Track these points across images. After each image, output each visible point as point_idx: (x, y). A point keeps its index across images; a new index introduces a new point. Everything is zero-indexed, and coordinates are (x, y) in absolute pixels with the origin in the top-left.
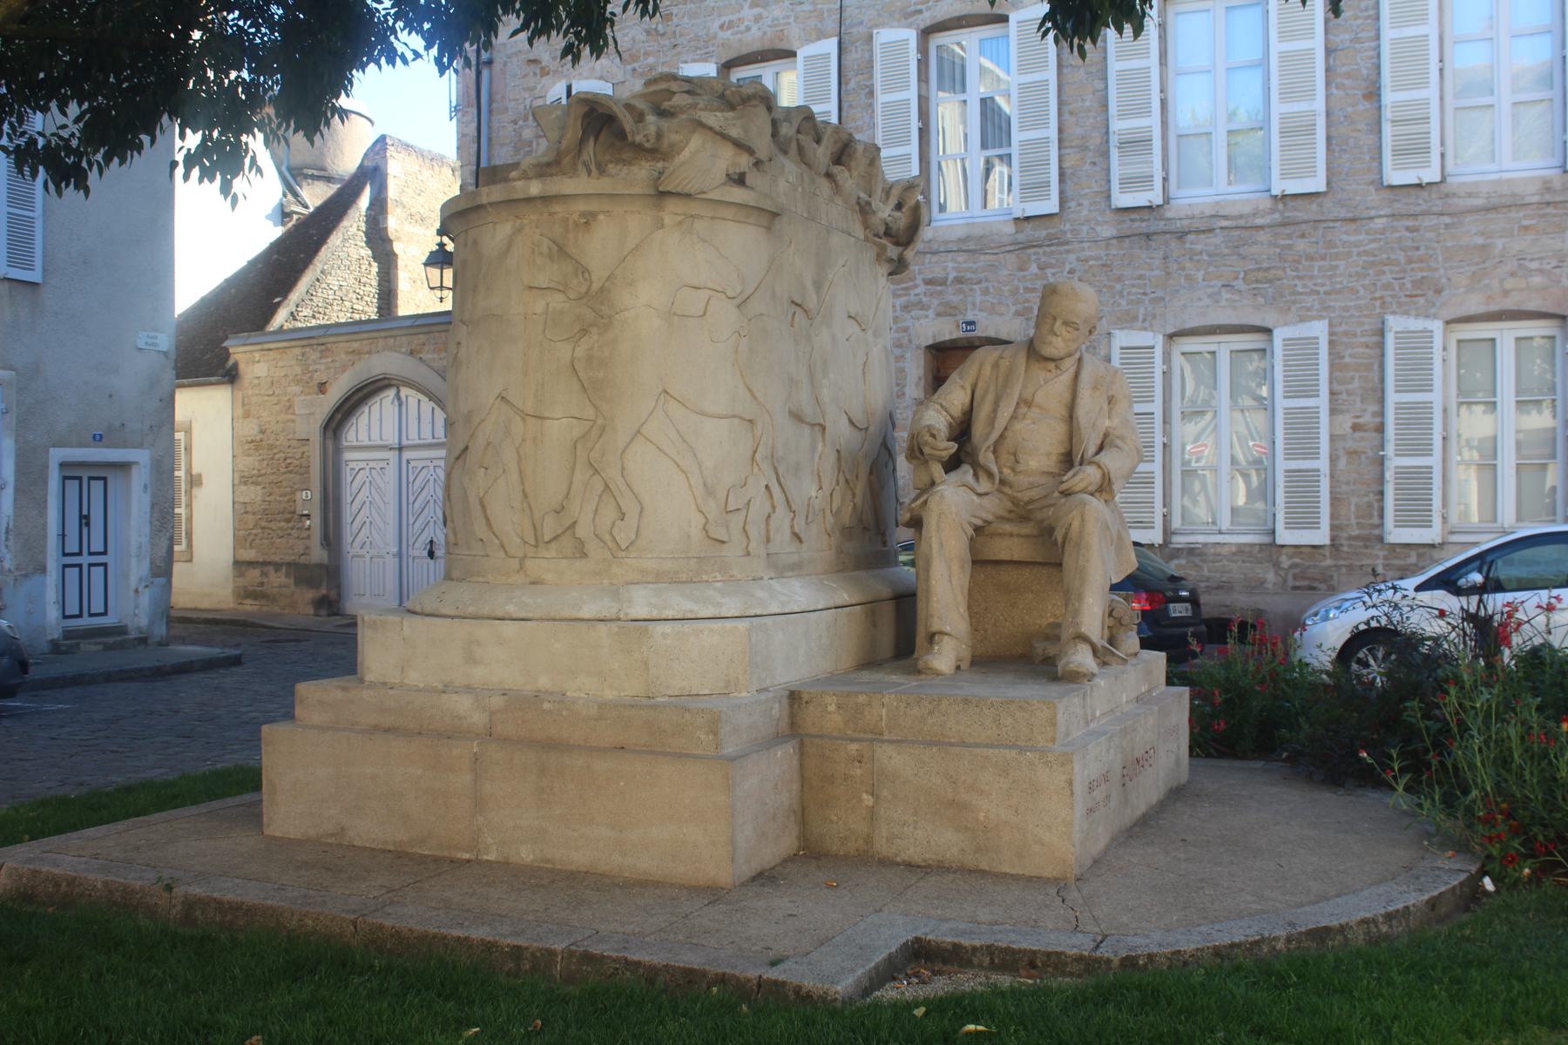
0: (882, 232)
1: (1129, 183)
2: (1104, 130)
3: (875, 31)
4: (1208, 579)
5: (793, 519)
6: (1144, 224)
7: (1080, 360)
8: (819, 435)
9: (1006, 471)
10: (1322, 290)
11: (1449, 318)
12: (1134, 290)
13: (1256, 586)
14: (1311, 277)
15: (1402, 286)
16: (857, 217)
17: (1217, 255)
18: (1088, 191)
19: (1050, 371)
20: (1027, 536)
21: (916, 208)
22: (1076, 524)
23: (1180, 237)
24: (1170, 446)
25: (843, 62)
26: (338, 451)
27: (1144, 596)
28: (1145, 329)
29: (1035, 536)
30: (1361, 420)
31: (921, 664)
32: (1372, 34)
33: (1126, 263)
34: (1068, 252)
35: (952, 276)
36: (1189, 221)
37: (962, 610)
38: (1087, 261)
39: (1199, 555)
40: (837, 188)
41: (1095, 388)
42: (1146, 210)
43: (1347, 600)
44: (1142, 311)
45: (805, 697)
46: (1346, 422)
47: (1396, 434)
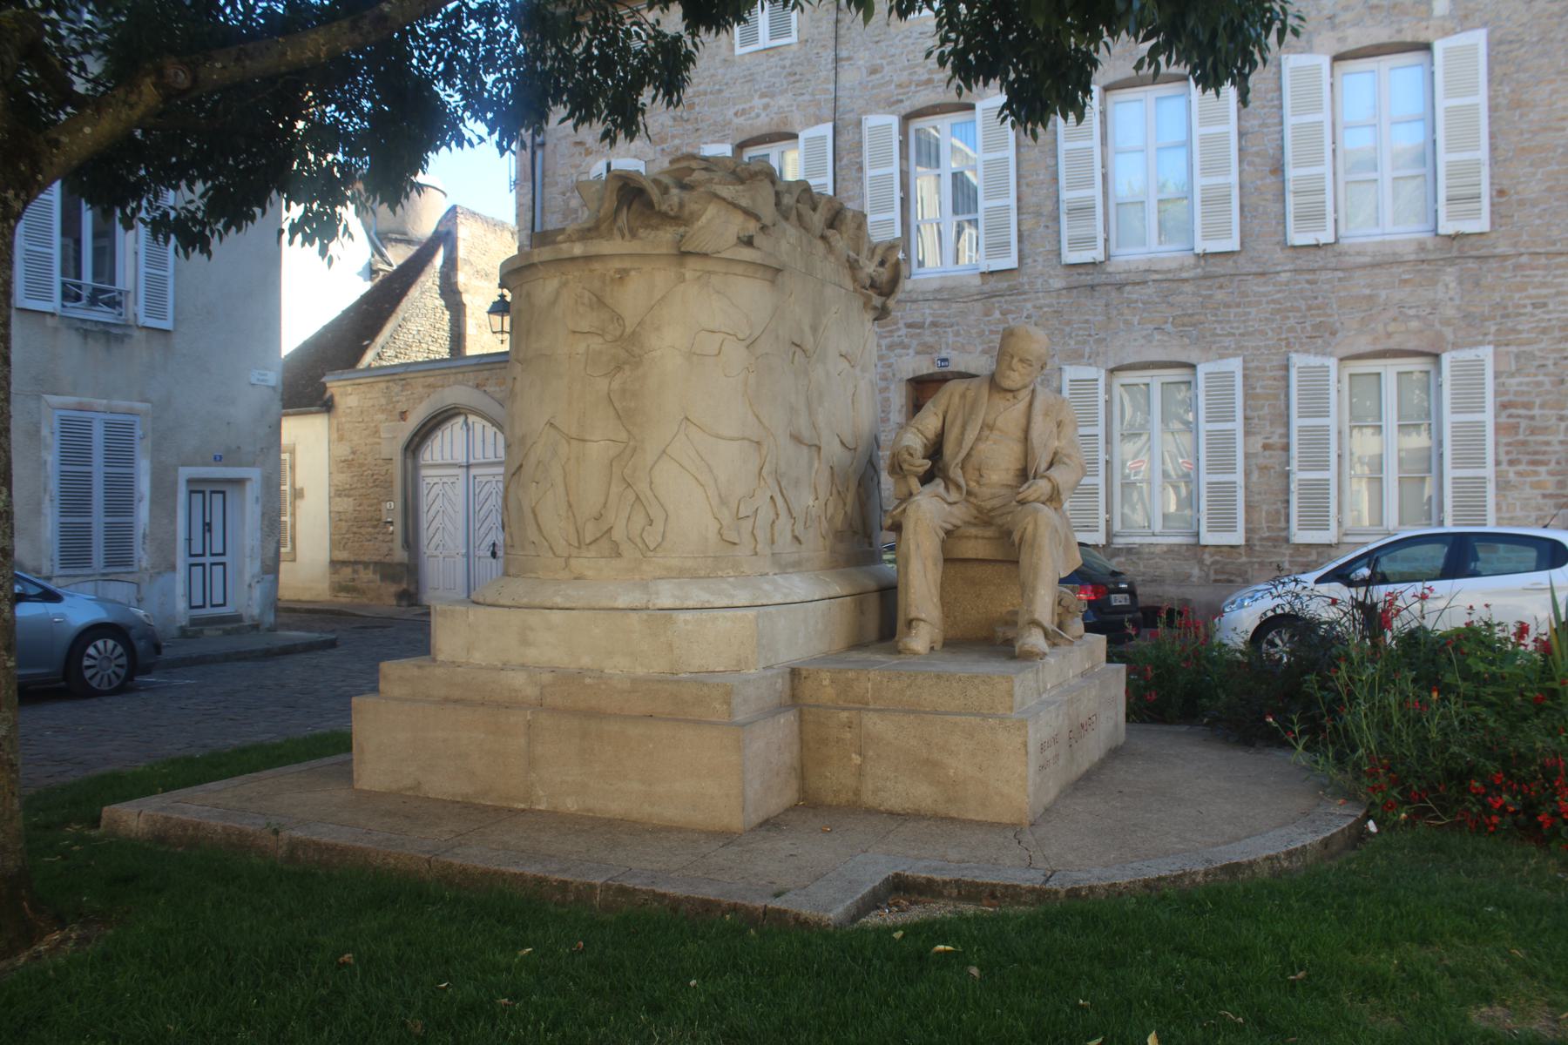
1: (1076, 243)
2: (1055, 199)
3: (864, 117)
4: (1144, 574)
5: (793, 525)
6: (1089, 278)
7: (1033, 391)
9: (973, 484)
10: (1237, 332)
11: (1342, 356)
12: (1081, 333)
13: (1184, 579)
16: (847, 272)
17: (1149, 303)
20: (989, 539)
22: (1030, 528)
24: (1112, 463)
26: (416, 468)
28: (1090, 365)
30: (1270, 441)
31: (901, 645)
32: (1276, 120)
34: (1025, 300)
40: (830, 248)
44: (1087, 350)
45: (804, 673)
46: (1257, 442)
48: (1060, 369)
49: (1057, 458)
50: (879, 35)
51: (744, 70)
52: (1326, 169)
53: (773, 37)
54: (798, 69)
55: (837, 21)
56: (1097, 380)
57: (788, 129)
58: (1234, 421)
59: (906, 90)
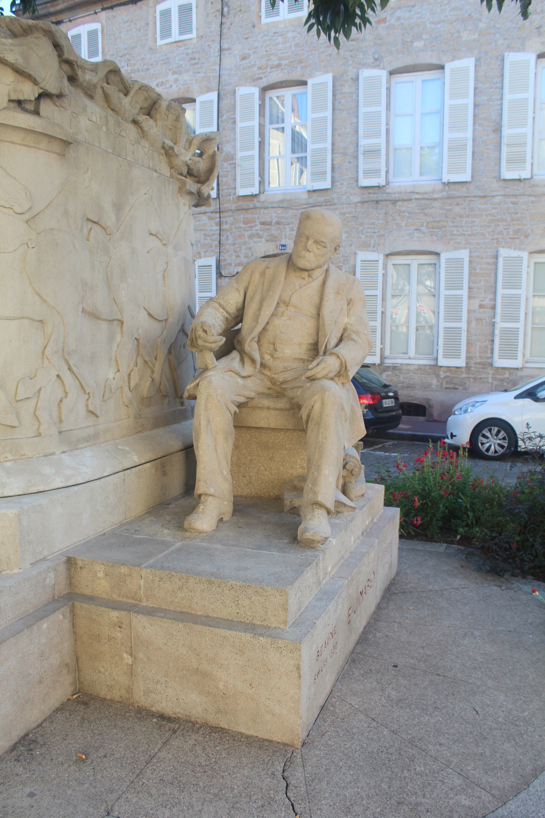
1: (368, 173)
2: (356, 145)
3: (237, 88)
4: (403, 382)
5: (87, 400)
6: (375, 196)
7: (327, 271)
8: (118, 329)
9: (267, 357)
10: (466, 233)
11: (531, 251)
12: (369, 230)
13: (427, 387)
14: (461, 227)
15: (508, 233)
16: (163, 158)
19: (304, 279)
20: (281, 409)
21: (213, 157)
22: (317, 407)
23: (394, 203)
24: (385, 313)
25: (220, 105)
27: (370, 396)
28: (374, 251)
30: (484, 303)
32: (499, 97)
33: (365, 216)
34: (335, 209)
35: (274, 220)
37: (225, 473)
39: (398, 370)
40: (143, 134)
41: (338, 293)
43: (478, 402)
44: (373, 241)
45: (80, 563)
46: (476, 303)
47: (502, 311)
48: (355, 253)
50: (248, 33)
51: (162, 56)
52: (528, 130)
53: (181, 33)
54: (197, 56)
55: (222, 24)
56: (378, 261)
57: (190, 96)
58: (462, 289)
59: (264, 71)
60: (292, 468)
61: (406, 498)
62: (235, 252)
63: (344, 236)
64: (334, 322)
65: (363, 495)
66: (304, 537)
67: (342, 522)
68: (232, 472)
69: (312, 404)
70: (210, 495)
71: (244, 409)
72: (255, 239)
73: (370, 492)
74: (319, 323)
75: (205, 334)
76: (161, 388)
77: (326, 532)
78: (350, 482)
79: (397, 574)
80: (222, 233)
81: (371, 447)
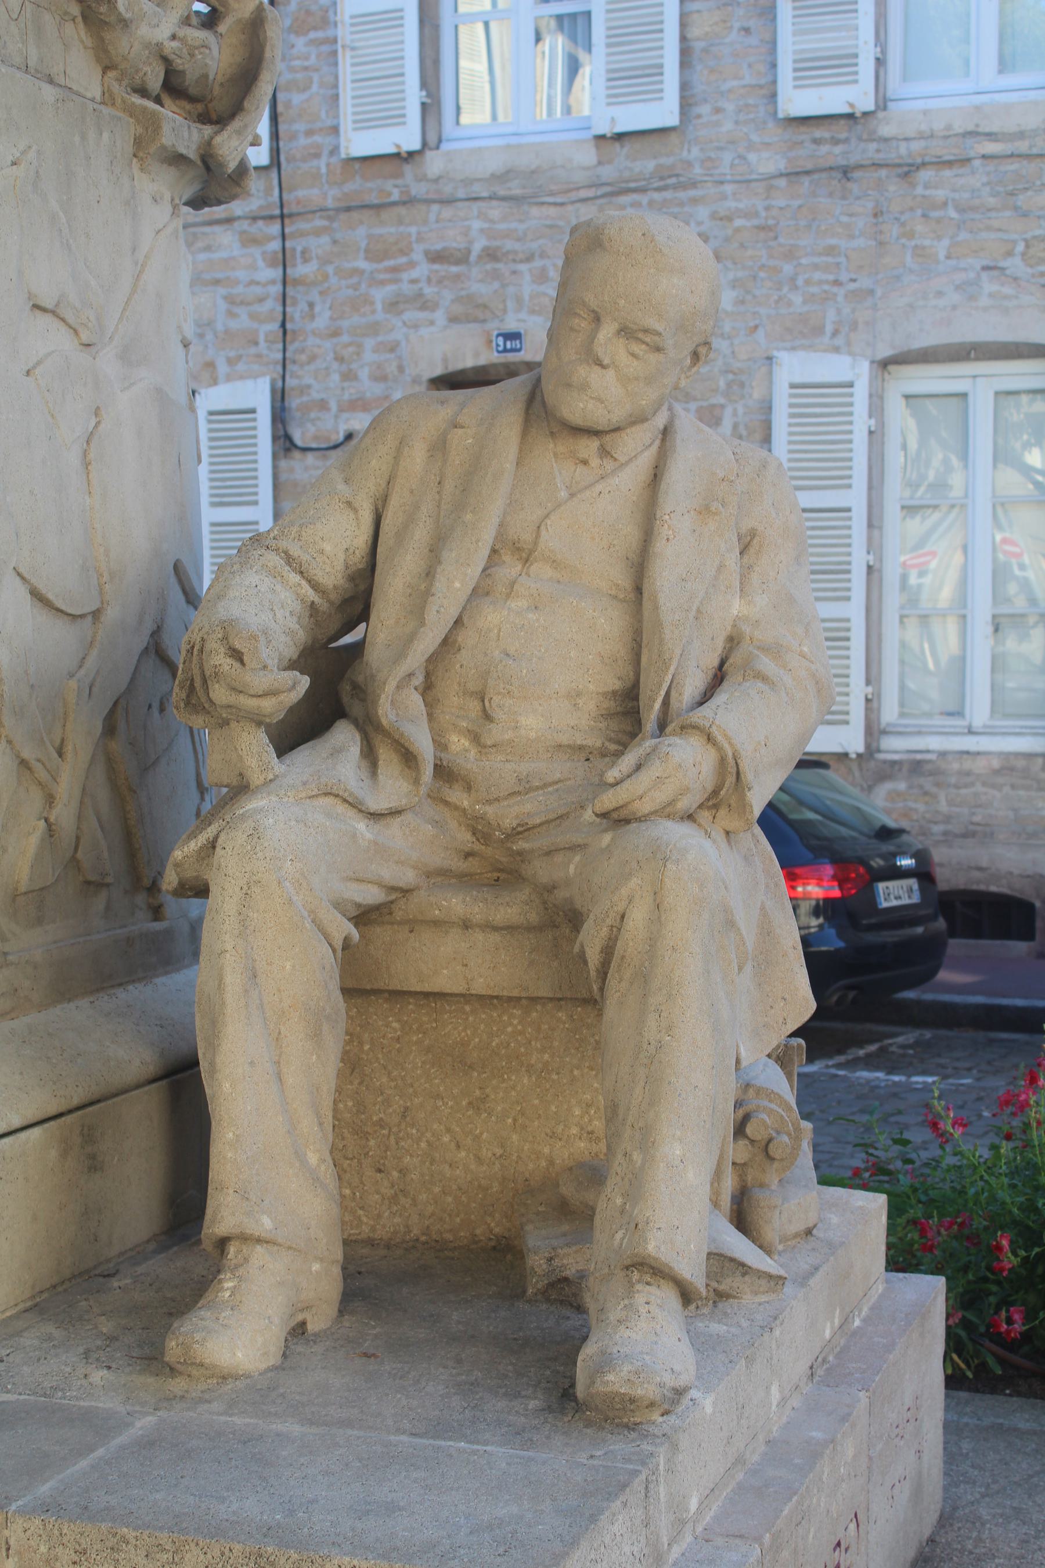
0: (155, 83)
4: (948, 819)
6: (838, 149)
7: (666, 432)
9: (458, 743)
12: (817, 276)
17: (974, 209)
18: (735, 83)
19: (585, 462)
20: (510, 929)
22: (638, 917)
23: (907, 174)
24: (880, 571)
27: (829, 870)
28: (837, 350)
29: (530, 929)
31: (173, 1348)
33: (803, 223)
34: (694, 201)
35: (479, 246)
36: (922, 143)
37: (313, 1159)
38: (729, 219)
39: (931, 774)
41: (705, 511)
42: (842, 122)
44: (831, 316)
48: (770, 358)
49: (735, 659)
56: (851, 385)
60: (553, 1135)
61: (968, 1238)
62: (339, 359)
63: (727, 299)
64: (693, 613)
65: (809, 1232)
66: (599, 1387)
67: (734, 1330)
68: (338, 1155)
69: (620, 908)
70: (259, 1241)
71: (378, 930)
72: (412, 315)
73: (835, 1220)
74: (640, 621)
75: (237, 665)
76: (80, 855)
77: (677, 1368)
78: (762, 1185)
79: (944, 1521)
80: (290, 291)
81: (840, 1052)
